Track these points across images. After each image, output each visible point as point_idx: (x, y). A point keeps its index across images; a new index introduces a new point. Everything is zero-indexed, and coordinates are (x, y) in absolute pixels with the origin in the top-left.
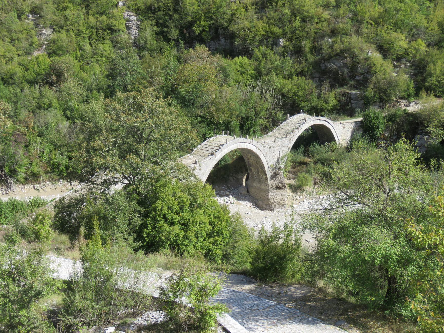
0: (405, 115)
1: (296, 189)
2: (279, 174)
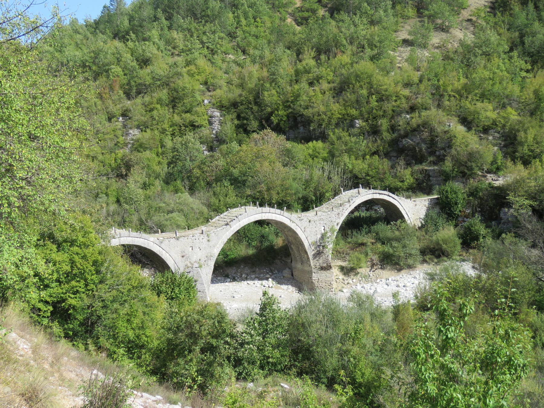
0: (489, 189)
1: (347, 271)
2: (322, 252)
